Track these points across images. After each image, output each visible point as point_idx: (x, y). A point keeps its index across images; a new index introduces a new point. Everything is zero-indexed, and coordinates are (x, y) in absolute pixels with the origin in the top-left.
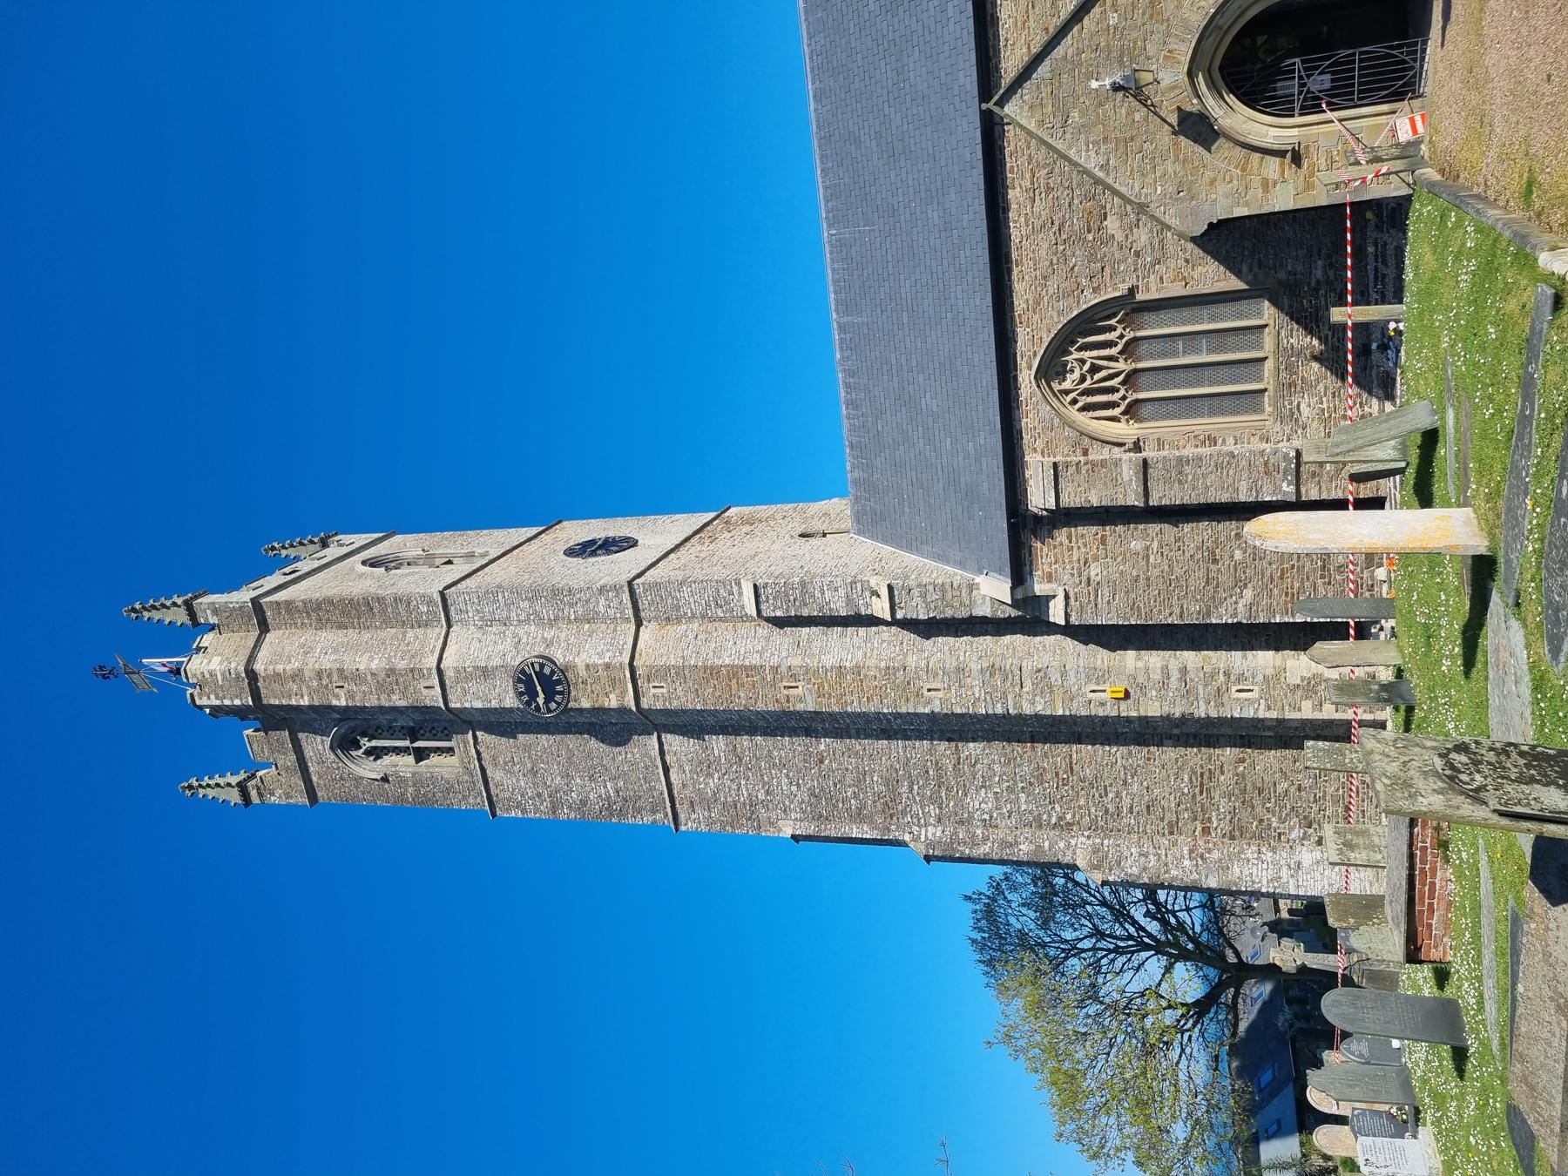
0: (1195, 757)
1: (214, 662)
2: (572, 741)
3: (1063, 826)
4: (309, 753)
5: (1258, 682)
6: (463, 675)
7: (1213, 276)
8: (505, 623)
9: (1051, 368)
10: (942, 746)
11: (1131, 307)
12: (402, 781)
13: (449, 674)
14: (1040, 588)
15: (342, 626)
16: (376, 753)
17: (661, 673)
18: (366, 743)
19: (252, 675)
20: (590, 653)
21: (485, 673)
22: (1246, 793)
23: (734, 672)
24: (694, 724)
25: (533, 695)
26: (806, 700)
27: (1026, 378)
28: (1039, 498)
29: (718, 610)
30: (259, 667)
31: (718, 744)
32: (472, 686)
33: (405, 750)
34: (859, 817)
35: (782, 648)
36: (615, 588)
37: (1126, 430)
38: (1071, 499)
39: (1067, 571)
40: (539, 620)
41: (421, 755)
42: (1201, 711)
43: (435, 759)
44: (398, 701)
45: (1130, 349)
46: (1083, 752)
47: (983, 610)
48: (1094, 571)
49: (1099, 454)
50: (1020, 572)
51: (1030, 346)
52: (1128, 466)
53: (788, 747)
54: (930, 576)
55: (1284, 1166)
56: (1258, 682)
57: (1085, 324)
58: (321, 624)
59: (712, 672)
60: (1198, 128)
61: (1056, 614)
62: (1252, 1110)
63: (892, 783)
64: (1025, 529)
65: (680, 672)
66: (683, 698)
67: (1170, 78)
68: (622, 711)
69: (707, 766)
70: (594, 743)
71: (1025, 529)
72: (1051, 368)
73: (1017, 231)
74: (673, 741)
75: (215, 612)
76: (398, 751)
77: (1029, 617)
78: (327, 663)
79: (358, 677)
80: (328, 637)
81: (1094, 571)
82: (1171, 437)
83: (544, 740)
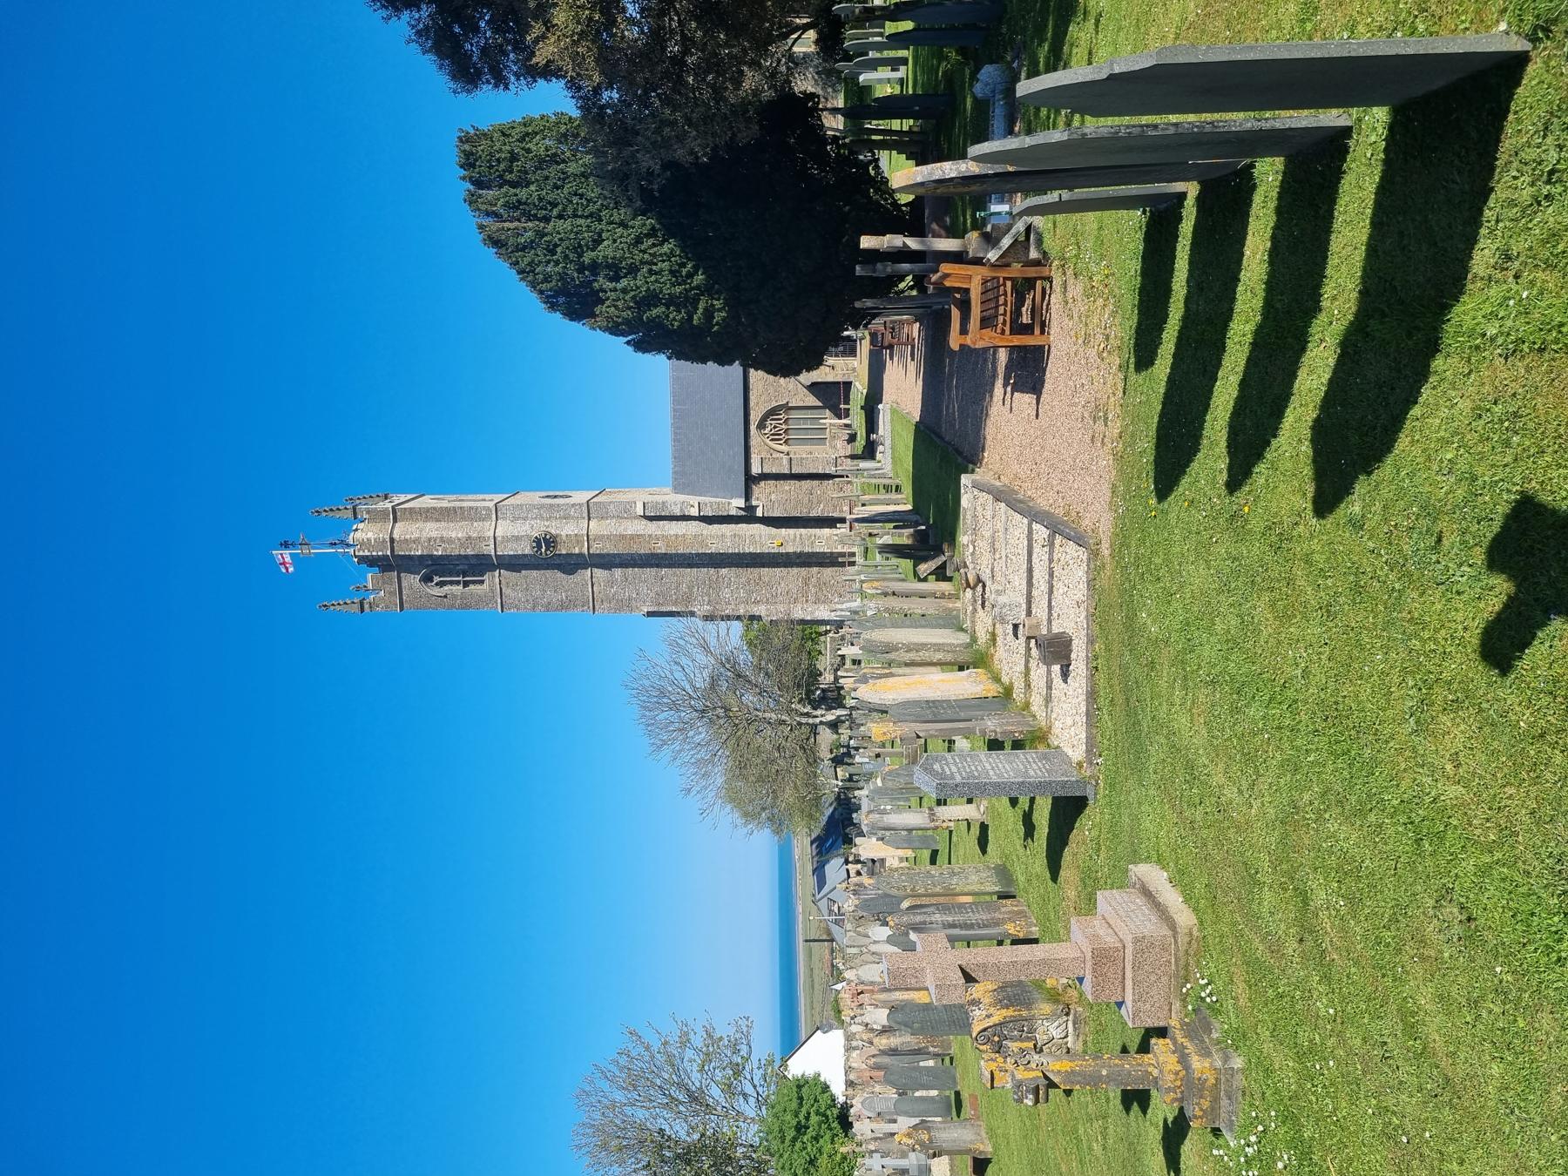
0: (803, 571)
1: (367, 534)
2: (548, 573)
3: (756, 602)
4: (404, 584)
5: (822, 540)
6: (506, 539)
7: (812, 401)
8: (525, 519)
10: (712, 571)
11: (787, 408)
12: (455, 596)
14: (754, 503)
15: (438, 520)
16: (441, 584)
17: (600, 538)
18: (437, 579)
19: (392, 540)
20: (569, 531)
21: (517, 538)
22: (821, 585)
23: (632, 537)
24: (606, 562)
25: (539, 547)
26: (661, 548)
27: (753, 428)
28: (756, 469)
29: (625, 513)
30: (396, 536)
31: (618, 572)
33: (458, 583)
34: (675, 603)
35: (653, 528)
36: (581, 505)
37: (784, 448)
39: (767, 499)
40: (542, 518)
41: (466, 584)
43: (472, 587)
44: (470, 552)
46: (765, 571)
47: (733, 512)
48: (773, 497)
49: (776, 455)
50: (748, 497)
51: (755, 417)
53: (649, 572)
54: (712, 503)
55: (874, 16)
56: (822, 540)
57: (772, 412)
58: (427, 519)
59: (623, 537)
61: (759, 513)
62: (819, 853)
63: (690, 588)
64: (750, 480)
65: (608, 537)
66: (609, 549)
68: (581, 555)
69: (611, 583)
70: (559, 574)
71: (750, 480)
72: (761, 426)
74: (598, 572)
75: (368, 512)
76: (451, 583)
77: (749, 516)
78: (434, 534)
79: (450, 541)
80: (430, 525)
81: (773, 497)
82: (799, 451)
83: (535, 573)
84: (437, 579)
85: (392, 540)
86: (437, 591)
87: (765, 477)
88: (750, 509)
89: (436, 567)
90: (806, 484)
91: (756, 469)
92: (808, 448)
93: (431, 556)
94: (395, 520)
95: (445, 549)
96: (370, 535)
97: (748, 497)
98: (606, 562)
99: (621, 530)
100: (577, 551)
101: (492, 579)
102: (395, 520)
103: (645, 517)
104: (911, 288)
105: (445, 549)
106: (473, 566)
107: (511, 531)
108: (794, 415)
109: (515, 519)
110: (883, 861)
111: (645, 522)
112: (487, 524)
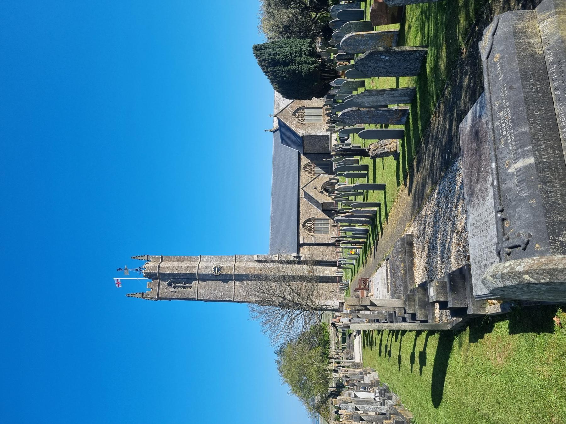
1: (151, 266)
4: (161, 286)
6: (202, 268)
9: (304, 225)
12: (179, 292)
13: (200, 267)
14: (300, 255)
15: (178, 261)
16: (175, 287)
17: (239, 268)
18: (173, 285)
19: (159, 267)
21: (207, 267)
27: (301, 226)
28: (301, 241)
30: (161, 265)
32: (204, 270)
33: (181, 287)
37: (313, 234)
38: (306, 242)
39: (305, 252)
41: (185, 287)
42: (321, 275)
43: (187, 289)
44: (188, 272)
45: (313, 224)
47: (292, 259)
49: (309, 236)
50: (298, 253)
51: (301, 222)
52: (313, 238)
57: (308, 221)
59: (248, 268)
60: (322, 192)
61: (302, 259)
64: (299, 246)
65: (242, 267)
66: (242, 272)
67: (319, 189)
68: (231, 275)
71: (299, 246)
73: (301, 209)
76: (179, 287)
78: (175, 265)
79: (181, 268)
84: (173, 285)
85: (159, 267)
86: (173, 290)
87: (305, 244)
88: (298, 257)
89: (175, 279)
90: (321, 248)
91: (301, 241)
92: (322, 234)
93: (172, 274)
94: (162, 261)
95: (179, 271)
96: (151, 265)
97: (298, 253)
98: (239, 278)
99: (248, 265)
100: (229, 273)
101: (195, 284)
102: (162, 261)
103: (257, 261)
104: (317, 15)
105: (179, 271)
106: (187, 279)
107: (206, 265)
108: (317, 222)
109: (207, 261)
110: (258, 49)
111: (257, 263)
112: (196, 263)
